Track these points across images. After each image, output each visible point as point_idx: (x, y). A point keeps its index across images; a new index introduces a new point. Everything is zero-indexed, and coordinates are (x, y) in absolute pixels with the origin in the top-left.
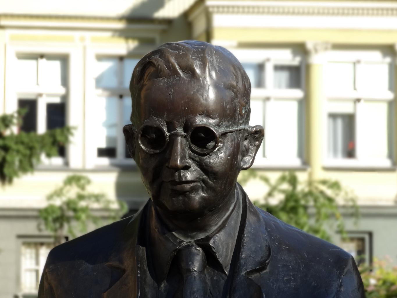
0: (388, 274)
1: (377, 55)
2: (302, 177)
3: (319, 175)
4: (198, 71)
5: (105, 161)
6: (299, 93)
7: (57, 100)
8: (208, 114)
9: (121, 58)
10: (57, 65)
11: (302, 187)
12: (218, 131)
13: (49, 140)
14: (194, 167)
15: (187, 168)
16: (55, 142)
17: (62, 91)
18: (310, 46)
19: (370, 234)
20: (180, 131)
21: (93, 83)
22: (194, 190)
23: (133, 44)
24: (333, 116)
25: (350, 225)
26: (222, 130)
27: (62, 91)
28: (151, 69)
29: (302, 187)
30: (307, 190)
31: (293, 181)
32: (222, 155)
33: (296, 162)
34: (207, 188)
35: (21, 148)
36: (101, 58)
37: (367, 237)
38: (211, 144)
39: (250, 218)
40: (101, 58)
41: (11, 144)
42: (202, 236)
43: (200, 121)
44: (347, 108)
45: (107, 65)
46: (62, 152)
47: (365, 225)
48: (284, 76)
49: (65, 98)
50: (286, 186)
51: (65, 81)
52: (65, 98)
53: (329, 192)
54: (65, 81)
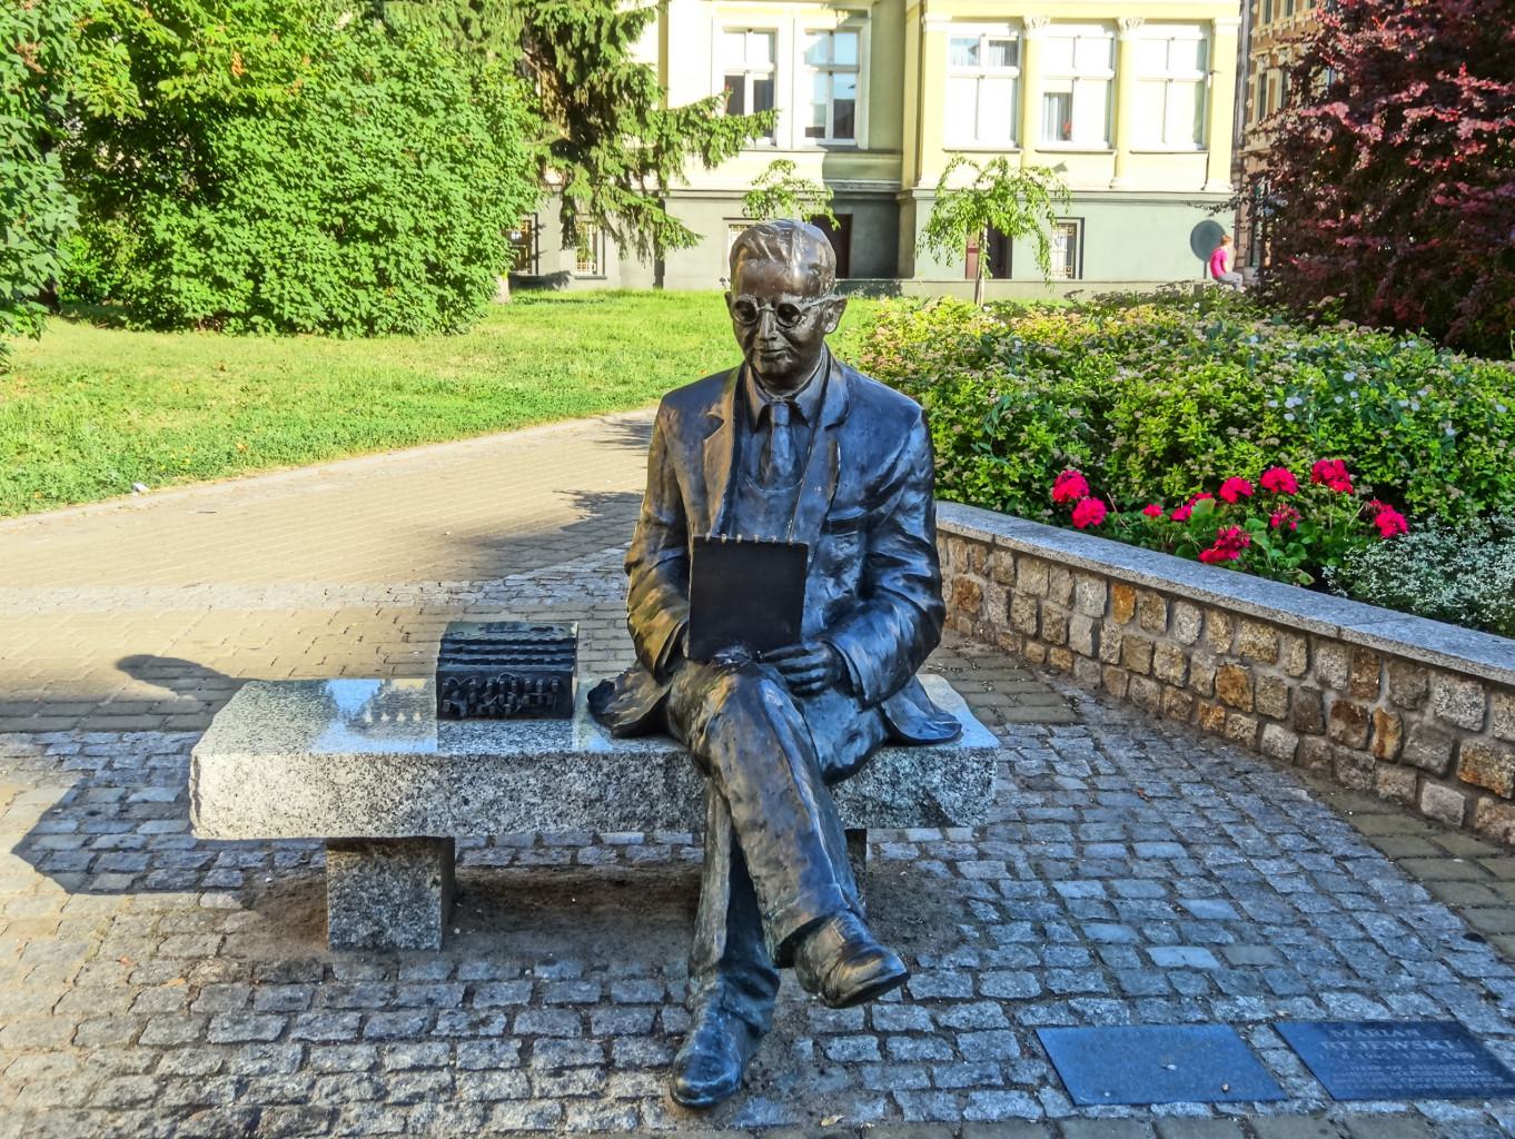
0: (809, 613)
1: (1099, 29)
2: (1013, 161)
3: (1032, 159)
4: (784, 253)
5: (813, 141)
6: (1014, 71)
7: (765, 77)
8: (793, 292)
9: (831, 33)
10: (766, 38)
11: (1013, 174)
12: (800, 308)
13: (753, 123)
14: (780, 337)
15: (774, 339)
16: (760, 125)
17: (770, 67)
18: (1027, 21)
19: (1083, 220)
20: (768, 306)
21: (800, 59)
22: (779, 357)
23: (843, 17)
24: (1049, 95)
25: (1059, 210)
26: (806, 305)
27: (770, 67)
28: (744, 251)
29: (1013, 174)
30: (1017, 176)
31: (1004, 166)
32: (805, 326)
33: (1010, 145)
34: (793, 355)
35: (726, 131)
36: (812, 33)
37: (1079, 222)
38: (795, 318)
39: (834, 375)
40: (812, 33)
41: (715, 127)
42: (790, 394)
43: (786, 299)
44: (1065, 88)
45: (818, 38)
46: (769, 133)
47: (1076, 210)
48: (1001, 51)
49: (772, 74)
50: (996, 172)
51: (773, 59)
52: (772, 74)
53: (1039, 180)
54: (773, 59)
